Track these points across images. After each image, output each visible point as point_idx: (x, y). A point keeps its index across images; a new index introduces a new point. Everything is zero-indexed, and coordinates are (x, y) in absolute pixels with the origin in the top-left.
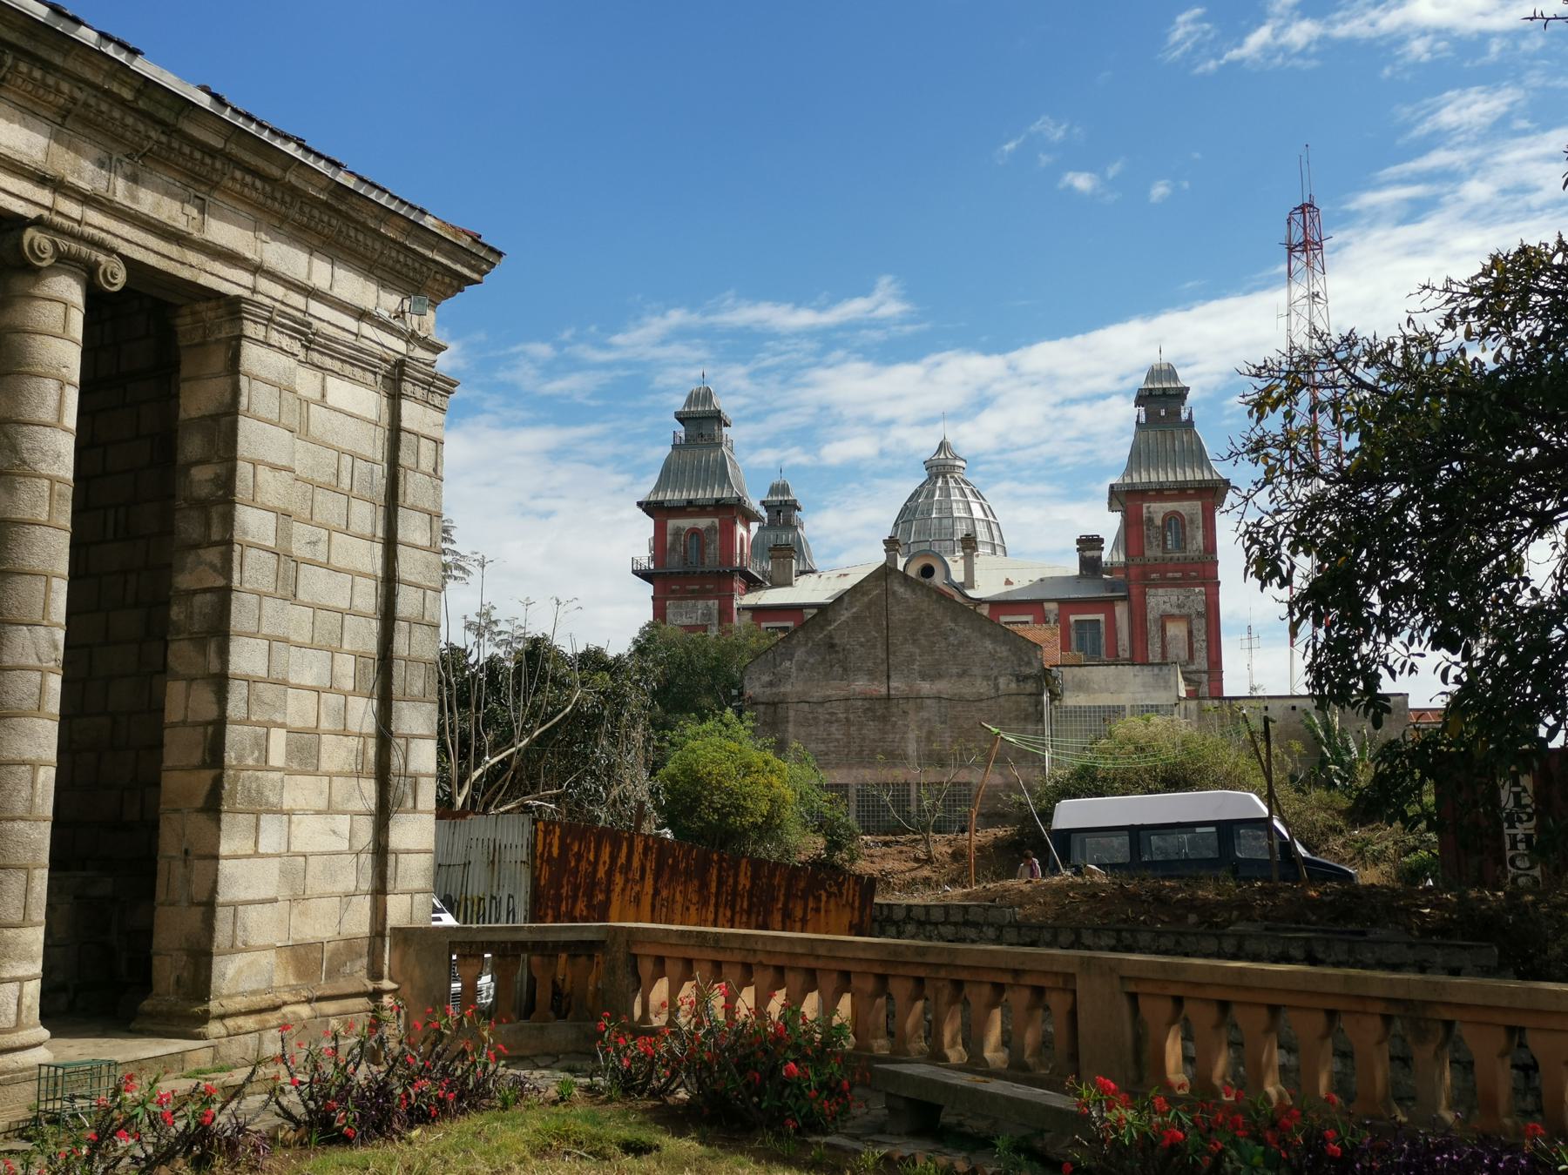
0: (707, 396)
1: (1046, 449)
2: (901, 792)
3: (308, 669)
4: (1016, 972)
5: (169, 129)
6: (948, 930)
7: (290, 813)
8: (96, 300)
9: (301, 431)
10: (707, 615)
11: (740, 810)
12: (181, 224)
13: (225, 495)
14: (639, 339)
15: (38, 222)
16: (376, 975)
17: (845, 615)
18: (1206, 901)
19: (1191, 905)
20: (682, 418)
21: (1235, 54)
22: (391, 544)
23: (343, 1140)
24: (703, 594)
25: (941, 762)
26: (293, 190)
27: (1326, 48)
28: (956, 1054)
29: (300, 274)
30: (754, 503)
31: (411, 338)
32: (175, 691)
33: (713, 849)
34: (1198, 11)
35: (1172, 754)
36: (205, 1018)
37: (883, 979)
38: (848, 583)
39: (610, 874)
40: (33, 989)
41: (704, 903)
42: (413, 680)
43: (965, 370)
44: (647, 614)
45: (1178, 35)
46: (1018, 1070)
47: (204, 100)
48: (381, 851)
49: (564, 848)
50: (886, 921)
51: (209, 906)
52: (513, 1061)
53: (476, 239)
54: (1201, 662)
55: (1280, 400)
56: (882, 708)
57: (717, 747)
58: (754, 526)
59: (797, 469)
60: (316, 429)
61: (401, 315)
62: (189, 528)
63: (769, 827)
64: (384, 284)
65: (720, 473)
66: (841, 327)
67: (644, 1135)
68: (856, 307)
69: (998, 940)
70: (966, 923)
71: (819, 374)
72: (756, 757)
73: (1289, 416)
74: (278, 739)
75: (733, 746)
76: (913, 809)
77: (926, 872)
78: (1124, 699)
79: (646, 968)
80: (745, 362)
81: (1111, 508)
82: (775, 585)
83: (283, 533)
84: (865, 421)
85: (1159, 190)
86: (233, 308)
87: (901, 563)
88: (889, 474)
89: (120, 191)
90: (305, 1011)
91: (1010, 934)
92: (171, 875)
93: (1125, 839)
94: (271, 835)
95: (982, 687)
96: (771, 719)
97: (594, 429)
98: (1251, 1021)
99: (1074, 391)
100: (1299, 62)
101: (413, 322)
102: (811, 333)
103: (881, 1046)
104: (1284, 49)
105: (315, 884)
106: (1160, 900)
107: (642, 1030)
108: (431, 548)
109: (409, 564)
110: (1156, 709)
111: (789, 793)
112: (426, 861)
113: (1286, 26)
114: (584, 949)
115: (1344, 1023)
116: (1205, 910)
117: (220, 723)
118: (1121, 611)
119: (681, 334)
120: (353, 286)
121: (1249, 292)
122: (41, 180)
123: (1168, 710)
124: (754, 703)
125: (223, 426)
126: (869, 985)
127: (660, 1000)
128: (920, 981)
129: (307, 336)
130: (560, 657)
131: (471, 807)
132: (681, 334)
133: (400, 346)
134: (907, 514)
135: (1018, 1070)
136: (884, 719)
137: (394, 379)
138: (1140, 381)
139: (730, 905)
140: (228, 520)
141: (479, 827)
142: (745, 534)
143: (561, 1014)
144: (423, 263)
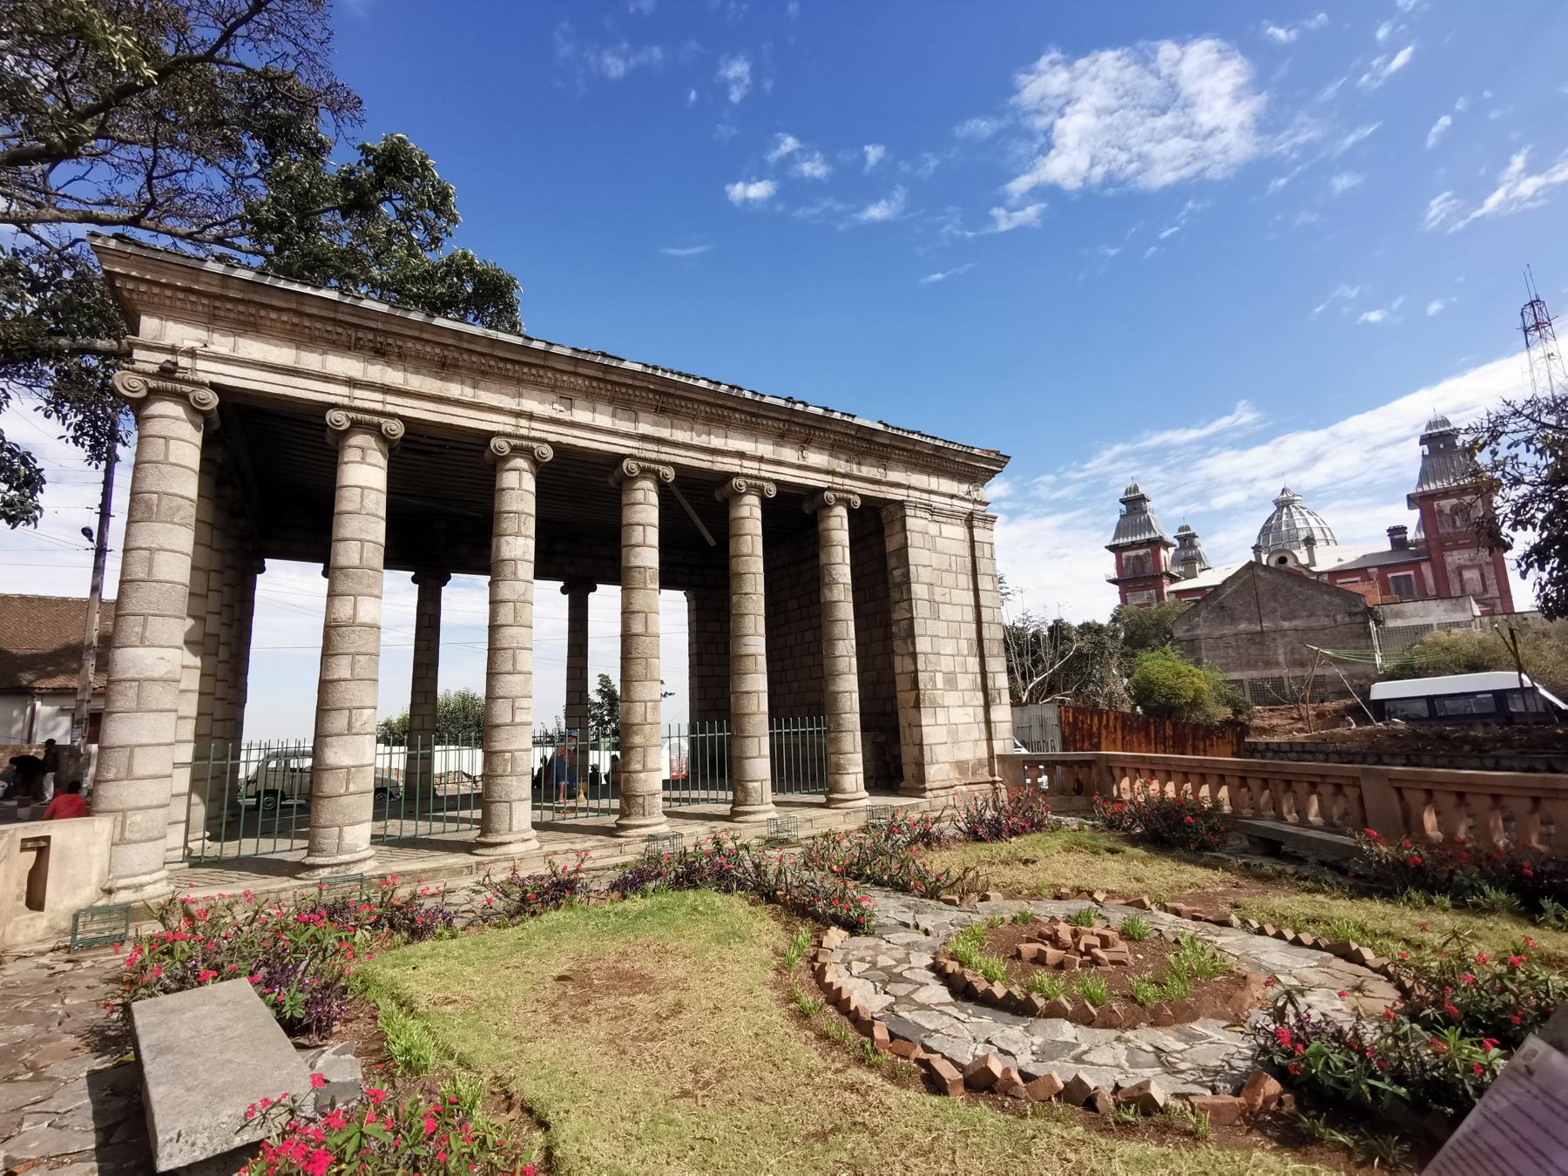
0: (1136, 489)
1: (1366, 478)
2: (1278, 683)
3: (948, 647)
4: (1323, 776)
5: (869, 441)
6: (1294, 755)
7: (124, 811)
8: (851, 512)
9: (933, 549)
10: (1150, 598)
11: (1177, 696)
12: (878, 477)
13: (907, 581)
14: (1098, 464)
15: (829, 489)
16: (993, 775)
17: (1229, 591)
18: (1475, 738)
19: (1466, 740)
20: (1123, 501)
21: (1479, 213)
22: (976, 591)
23: (981, 840)
24: (1146, 588)
25: (1303, 665)
26: (919, 453)
27: (1551, 191)
28: (1292, 817)
29: (925, 485)
30: (1169, 537)
31: (975, 501)
32: (898, 660)
33: (1164, 719)
34: (1447, 194)
35: (1469, 648)
36: (925, 790)
37: (1243, 780)
38: (1230, 573)
39: (1099, 729)
40: (861, 777)
41: (1149, 742)
42: (994, 648)
43: (1298, 444)
44: (1118, 601)
45: (1433, 213)
46: (1329, 826)
47: (881, 427)
48: (988, 722)
49: (1075, 718)
50: (1253, 750)
51: (921, 745)
52: (1054, 813)
53: (997, 453)
54: (1494, 591)
55: (1485, 444)
56: (1259, 638)
57: (1160, 664)
58: (1172, 550)
59: (1197, 515)
60: (939, 547)
61: (969, 493)
62: (895, 595)
63: (1195, 704)
64: (960, 481)
65: (1148, 526)
66: (1215, 435)
67: (1117, 846)
68: (1224, 422)
69: (1327, 761)
70: (1305, 752)
71: (1204, 462)
72: (1183, 668)
73: (1494, 453)
74: (939, 678)
75: (1169, 664)
76: (1287, 691)
77: (1300, 725)
78: (1432, 620)
79: (1117, 773)
80: (1158, 464)
81: (1410, 507)
82: (1187, 578)
83: (931, 592)
84: (1237, 482)
85: (1434, 308)
86: (901, 505)
87: (1264, 558)
88: (1256, 508)
89: (855, 470)
90: (964, 788)
91: (1335, 757)
92: (905, 733)
93: (1424, 704)
94: (941, 716)
95: (1325, 622)
96: (1191, 649)
97: (1080, 512)
98: (1480, 804)
99: (1381, 440)
100: (1529, 205)
101: (974, 495)
102: (1196, 442)
103: (1247, 812)
104: (1519, 200)
105: (962, 737)
106: (1442, 738)
107: (1118, 800)
108: (995, 590)
109: (985, 599)
110: (1457, 625)
111: (1205, 686)
112: (1009, 725)
113: (1517, 185)
114: (1088, 764)
115: (1544, 803)
116: (1474, 742)
117: (916, 672)
118: (1426, 569)
119: (1121, 457)
120: (947, 485)
121: (1512, 355)
122: (828, 472)
123: (1468, 624)
124: (1180, 641)
125: (903, 550)
126: (1236, 782)
127: (1126, 788)
128: (1265, 780)
129: (931, 510)
130: (1069, 627)
131: (1031, 700)
132: (1121, 457)
133: (970, 506)
134: (1266, 531)
135: (1329, 826)
136: (1262, 643)
137: (970, 520)
138: (1422, 430)
139: (1162, 743)
140: (909, 590)
141: (1034, 710)
142: (1166, 555)
143: (1078, 793)
144: (973, 468)
